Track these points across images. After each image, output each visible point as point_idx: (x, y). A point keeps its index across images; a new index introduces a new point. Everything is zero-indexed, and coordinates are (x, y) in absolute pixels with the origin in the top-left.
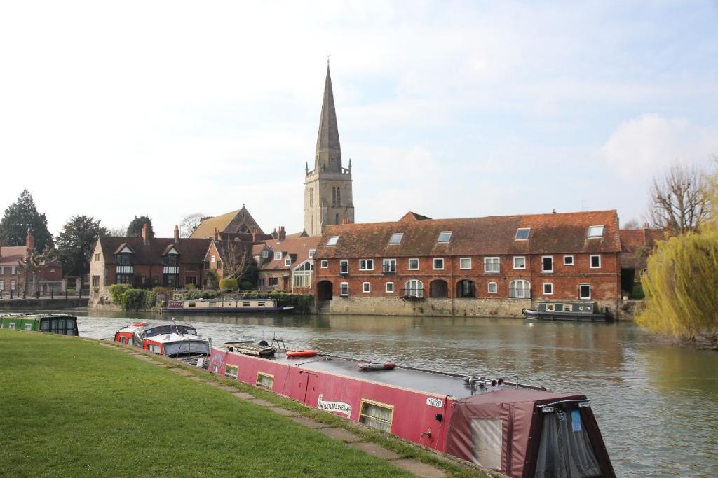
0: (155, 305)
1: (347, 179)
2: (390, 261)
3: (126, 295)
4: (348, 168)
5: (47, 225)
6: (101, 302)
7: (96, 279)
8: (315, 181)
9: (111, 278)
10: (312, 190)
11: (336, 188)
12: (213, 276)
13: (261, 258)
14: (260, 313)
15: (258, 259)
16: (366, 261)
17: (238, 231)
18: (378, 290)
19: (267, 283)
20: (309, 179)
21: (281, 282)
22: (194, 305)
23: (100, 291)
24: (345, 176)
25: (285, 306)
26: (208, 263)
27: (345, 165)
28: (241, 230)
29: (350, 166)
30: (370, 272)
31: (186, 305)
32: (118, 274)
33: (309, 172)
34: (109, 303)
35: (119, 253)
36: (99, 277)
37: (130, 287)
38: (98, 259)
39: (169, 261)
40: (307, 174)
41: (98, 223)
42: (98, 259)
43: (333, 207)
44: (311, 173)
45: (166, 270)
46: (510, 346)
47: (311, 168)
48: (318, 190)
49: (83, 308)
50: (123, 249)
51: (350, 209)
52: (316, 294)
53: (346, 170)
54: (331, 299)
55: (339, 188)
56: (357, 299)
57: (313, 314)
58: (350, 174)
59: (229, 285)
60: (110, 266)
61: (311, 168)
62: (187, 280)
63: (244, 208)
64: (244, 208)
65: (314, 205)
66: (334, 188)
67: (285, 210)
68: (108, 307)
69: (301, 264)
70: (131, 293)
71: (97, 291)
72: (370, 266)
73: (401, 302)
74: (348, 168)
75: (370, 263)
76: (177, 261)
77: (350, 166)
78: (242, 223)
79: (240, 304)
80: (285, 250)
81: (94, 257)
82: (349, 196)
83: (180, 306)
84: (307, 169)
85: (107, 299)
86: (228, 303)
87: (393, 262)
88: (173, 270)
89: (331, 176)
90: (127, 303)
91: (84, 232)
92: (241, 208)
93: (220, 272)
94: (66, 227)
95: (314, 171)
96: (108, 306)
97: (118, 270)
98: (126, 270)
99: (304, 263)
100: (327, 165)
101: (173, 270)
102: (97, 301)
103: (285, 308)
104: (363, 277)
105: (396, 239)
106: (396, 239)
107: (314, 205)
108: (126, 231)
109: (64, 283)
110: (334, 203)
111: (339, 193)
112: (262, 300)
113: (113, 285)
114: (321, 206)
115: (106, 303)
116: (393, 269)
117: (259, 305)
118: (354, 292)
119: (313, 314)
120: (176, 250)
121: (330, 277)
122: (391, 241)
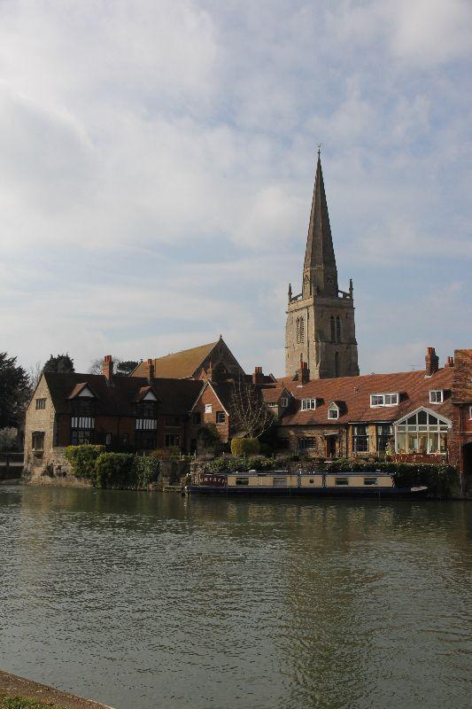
0: (156, 480)
1: (347, 305)
3: (103, 462)
6: (49, 471)
7: (38, 437)
8: (307, 307)
9: (64, 435)
10: (300, 320)
11: (335, 318)
12: (210, 437)
13: (280, 407)
15: (275, 409)
19: (294, 444)
20: (293, 306)
21: (322, 445)
22: (247, 483)
23: (45, 455)
24: (343, 301)
26: (199, 415)
27: (343, 286)
29: (351, 289)
32: (74, 429)
34: (65, 474)
35: (77, 398)
36: (43, 434)
37: (103, 450)
39: (143, 410)
40: (291, 300)
41: (13, 361)
43: (331, 343)
44: (296, 298)
46: (354, 562)
48: (312, 320)
49: (15, 480)
50: (80, 392)
51: (352, 346)
52: (461, 465)
53: (345, 294)
55: (338, 318)
57: (456, 500)
58: (352, 300)
59: (247, 449)
60: (61, 419)
61: (296, 291)
62: (167, 440)
63: (221, 341)
64: (221, 341)
65: (306, 339)
66: (332, 318)
68: (63, 481)
69: (410, 415)
70: (111, 460)
71: (39, 456)
74: (348, 292)
76: (155, 410)
77: (351, 289)
80: (320, 396)
81: (34, 403)
82: (351, 328)
83: (221, 484)
84: (290, 293)
85: (59, 468)
86: (309, 478)
88: (150, 424)
89: (325, 300)
90: (104, 476)
92: (217, 340)
93: (223, 428)
95: (302, 294)
96: (63, 479)
97: (74, 422)
98: (86, 422)
99: (416, 412)
100: (322, 286)
101: (150, 424)
102: (38, 471)
103: (413, 489)
107: (306, 339)
110: (333, 337)
111: (338, 323)
113: (72, 448)
114: (317, 341)
115: (60, 475)
119: (456, 500)
120: (155, 395)
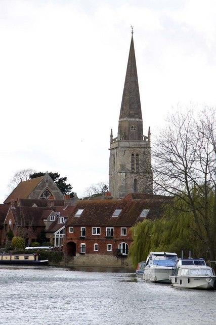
2: (110, 228)
4: (147, 136)
16: (96, 228)
17: (42, 196)
18: (102, 250)
25: (42, 260)
27: (145, 133)
28: (45, 194)
29: (149, 134)
30: (98, 236)
33: (114, 138)
47: (115, 135)
53: (146, 138)
54: (75, 255)
56: (91, 256)
67: (88, 173)
72: (98, 232)
73: (115, 258)
74: (147, 136)
75: (98, 229)
77: (149, 134)
78: (45, 189)
79: (13, 258)
84: (112, 136)
87: (112, 229)
104: (94, 240)
105: (117, 213)
106: (117, 213)
110: (133, 168)
112: (27, 255)
116: (112, 234)
117: (26, 258)
118: (89, 250)
121: (75, 239)
122: (114, 214)
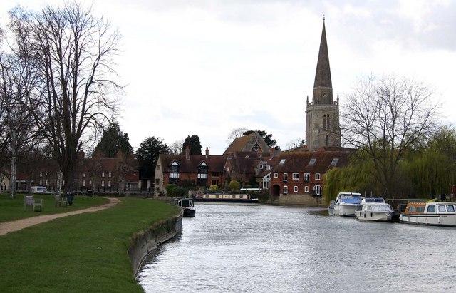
5: (129, 141)
7: (158, 180)
14: (241, 201)
18: (301, 191)
27: (335, 99)
29: (338, 99)
31: (204, 197)
38: (159, 169)
39: (202, 170)
42: (159, 169)
45: (199, 176)
56: (292, 195)
58: (338, 105)
67: (289, 132)
68: (165, 198)
72: (298, 177)
77: (338, 99)
79: (231, 197)
84: (308, 101)
91: (153, 148)
94: (142, 144)
101: (204, 176)
105: (312, 162)
106: (312, 162)
108: (181, 147)
109: (140, 183)
